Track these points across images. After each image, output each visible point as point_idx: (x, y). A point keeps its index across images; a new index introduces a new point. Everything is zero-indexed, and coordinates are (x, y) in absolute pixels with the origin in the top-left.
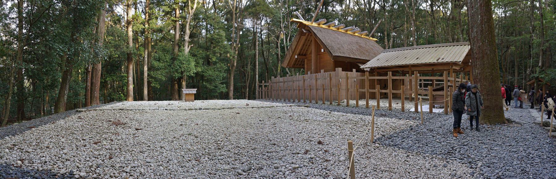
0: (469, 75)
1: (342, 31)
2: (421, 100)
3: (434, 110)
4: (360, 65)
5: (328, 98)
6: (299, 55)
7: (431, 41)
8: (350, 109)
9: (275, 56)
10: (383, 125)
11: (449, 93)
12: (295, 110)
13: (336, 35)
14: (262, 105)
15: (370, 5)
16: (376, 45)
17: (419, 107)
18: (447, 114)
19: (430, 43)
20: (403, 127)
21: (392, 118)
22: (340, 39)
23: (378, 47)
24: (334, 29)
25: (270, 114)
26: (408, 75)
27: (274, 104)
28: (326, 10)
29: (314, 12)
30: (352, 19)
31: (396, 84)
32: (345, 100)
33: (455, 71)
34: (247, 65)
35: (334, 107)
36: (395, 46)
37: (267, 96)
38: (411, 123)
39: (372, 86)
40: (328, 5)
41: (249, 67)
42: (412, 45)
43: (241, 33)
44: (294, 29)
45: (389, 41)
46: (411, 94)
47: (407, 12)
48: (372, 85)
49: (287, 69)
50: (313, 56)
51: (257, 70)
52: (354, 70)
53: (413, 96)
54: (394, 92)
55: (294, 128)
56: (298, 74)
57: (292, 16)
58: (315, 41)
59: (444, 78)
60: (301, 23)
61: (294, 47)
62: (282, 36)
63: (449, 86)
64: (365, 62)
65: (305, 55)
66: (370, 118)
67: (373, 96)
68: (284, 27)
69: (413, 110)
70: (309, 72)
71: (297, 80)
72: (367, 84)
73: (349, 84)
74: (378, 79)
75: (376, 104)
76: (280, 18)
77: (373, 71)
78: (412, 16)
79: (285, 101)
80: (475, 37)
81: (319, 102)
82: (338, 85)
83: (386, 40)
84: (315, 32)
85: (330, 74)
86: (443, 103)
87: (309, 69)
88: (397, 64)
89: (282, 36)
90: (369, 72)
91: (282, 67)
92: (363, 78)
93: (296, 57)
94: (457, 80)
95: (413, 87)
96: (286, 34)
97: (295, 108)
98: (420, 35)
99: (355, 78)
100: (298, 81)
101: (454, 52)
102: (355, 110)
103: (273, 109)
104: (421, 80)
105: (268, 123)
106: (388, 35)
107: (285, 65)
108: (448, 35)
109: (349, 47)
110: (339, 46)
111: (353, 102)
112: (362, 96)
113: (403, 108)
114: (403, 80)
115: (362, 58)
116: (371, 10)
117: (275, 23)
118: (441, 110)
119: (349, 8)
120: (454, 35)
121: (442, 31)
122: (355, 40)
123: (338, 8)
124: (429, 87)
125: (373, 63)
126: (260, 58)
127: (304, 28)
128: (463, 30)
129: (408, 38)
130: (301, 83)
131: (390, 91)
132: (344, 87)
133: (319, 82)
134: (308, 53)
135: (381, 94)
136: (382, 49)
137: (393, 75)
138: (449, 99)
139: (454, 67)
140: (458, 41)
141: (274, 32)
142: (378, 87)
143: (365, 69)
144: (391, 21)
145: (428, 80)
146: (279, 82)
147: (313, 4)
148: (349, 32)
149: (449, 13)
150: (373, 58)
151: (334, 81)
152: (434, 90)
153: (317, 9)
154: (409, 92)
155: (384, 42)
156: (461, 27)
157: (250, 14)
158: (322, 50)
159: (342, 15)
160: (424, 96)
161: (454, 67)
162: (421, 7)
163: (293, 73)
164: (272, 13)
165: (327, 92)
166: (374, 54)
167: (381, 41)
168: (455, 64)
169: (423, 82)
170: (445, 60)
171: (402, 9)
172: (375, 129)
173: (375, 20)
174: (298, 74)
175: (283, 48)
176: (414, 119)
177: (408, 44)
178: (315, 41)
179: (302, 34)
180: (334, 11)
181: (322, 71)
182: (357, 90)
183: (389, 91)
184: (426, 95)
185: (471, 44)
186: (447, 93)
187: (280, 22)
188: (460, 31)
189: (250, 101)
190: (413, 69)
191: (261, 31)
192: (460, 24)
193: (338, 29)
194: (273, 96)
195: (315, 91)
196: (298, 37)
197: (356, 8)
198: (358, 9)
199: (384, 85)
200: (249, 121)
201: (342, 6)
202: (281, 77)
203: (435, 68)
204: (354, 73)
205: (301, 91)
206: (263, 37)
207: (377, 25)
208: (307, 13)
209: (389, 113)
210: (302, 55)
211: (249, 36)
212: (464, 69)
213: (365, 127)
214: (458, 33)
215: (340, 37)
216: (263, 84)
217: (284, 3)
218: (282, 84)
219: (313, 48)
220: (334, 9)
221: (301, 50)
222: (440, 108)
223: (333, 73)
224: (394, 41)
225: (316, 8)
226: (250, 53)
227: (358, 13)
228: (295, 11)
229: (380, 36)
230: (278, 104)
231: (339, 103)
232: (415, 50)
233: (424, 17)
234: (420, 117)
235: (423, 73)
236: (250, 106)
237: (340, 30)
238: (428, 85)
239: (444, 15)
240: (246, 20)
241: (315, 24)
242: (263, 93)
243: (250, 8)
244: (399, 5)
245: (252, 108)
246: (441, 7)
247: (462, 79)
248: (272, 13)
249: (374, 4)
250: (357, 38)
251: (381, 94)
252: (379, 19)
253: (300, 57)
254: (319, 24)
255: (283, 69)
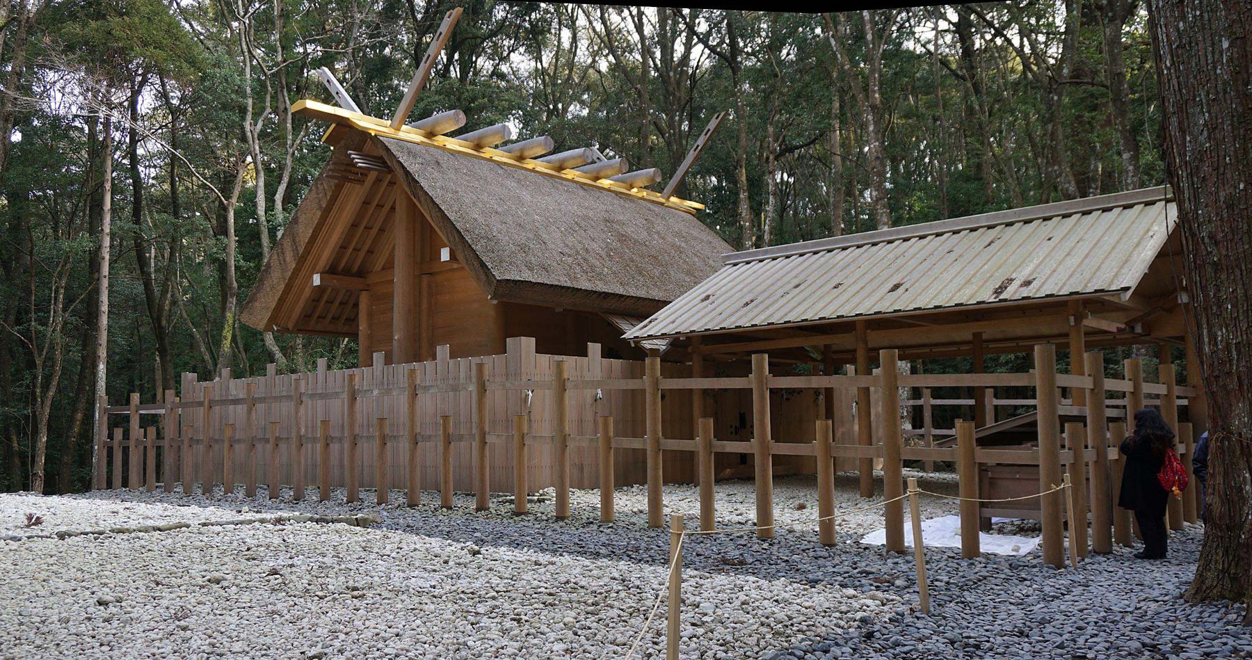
0: (1181, 355)
1: (540, 166)
2: (912, 489)
3: (989, 543)
4: (623, 325)
5: (466, 484)
6: (331, 271)
7: (963, 199)
8: (571, 533)
9: (208, 270)
10: (726, 612)
11: (1066, 456)
12: (303, 539)
13: (512, 184)
14: (118, 521)
15: (667, 51)
16: (700, 232)
17: (908, 526)
18: (1059, 565)
19: (958, 208)
20: (826, 625)
21: (771, 577)
22: (526, 203)
23: (708, 241)
24: (499, 156)
25: (160, 566)
26: (850, 368)
27: (193, 513)
28: (464, 72)
29: (407, 77)
30: (585, 112)
31: (792, 414)
32: (551, 491)
33: (1095, 340)
34: (43, 307)
35: (494, 525)
36: (789, 232)
37: (157, 473)
38: (869, 603)
39: (679, 424)
40: (476, 50)
41: (58, 317)
42: (872, 225)
43: (17, 137)
44: (312, 149)
45: (757, 209)
46: (870, 463)
47: (843, 75)
48: (679, 414)
49: (269, 339)
50: (400, 280)
51: (103, 338)
52: (595, 348)
53: (879, 469)
54: (785, 449)
55: (289, 631)
56: (322, 363)
57: (301, 90)
58: (412, 208)
59: (1035, 378)
60: (343, 123)
61: (304, 233)
62: (251, 178)
63: (1064, 419)
64: (644, 309)
65: (361, 273)
66: (666, 573)
67: (681, 472)
68: (263, 135)
69: (877, 537)
70: (378, 357)
71: (319, 393)
72: (653, 414)
73: (571, 414)
74: (706, 392)
75: (696, 509)
76: (240, 91)
77: (686, 351)
78: (866, 89)
79: (250, 494)
80: (1201, 155)
81: (424, 499)
82: (519, 417)
83: (744, 208)
84: (413, 167)
85: (480, 367)
86: (1035, 505)
87: (380, 340)
88: (795, 316)
89: (251, 178)
90: (666, 357)
91: (244, 327)
92: (632, 384)
93: (317, 280)
94: (1110, 384)
95: (880, 431)
96: (268, 170)
97: (303, 533)
98: (909, 173)
99: (595, 384)
100: (323, 396)
101: (1084, 248)
102: (594, 537)
103: (182, 537)
104: (916, 393)
105: (144, 613)
106: (756, 185)
107: (259, 316)
108: (1054, 160)
109: (570, 240)
110: (521, 238)
111: (585, 500)
112: (630, 473)
113: (827, 527)
114: (829, 392)
115: (632, 292)
116: (674, 71)
117: (208, 114)
118: (1028, 545)
119: (571, 65)
120: (1085, 159)
121: (1020, 146)
122: (597, 207)
123: (521, 62)
124: (958, 423)
125: (683, 315)
126: (125, 278)
127: (359, 149)
128: (1135, 131)
129: (849, 193)
130: (338, 407)
131: (764, 446)
132: (544, 426)
133: (426, 403)
134: (377, 270)
135: (722, 460)
136: (725, 249)
137: (776, 370)
138: (1067, 484)
139: (1091, 322)
140: (1110, 184)
141: (204, 154)
142: (705, 425)
143: (647, 345)
144: (765, 120)
145: (955, 392)
146: (223, 402)
147: (405, 38)
148: (570, 174)
149: (1055, 51)
150: (683, 289)
151: (496, 396)
152: (984, 442)
153: (423, 66)
154: (861, 451)
155: (735, 215)
156: (1122, 114)
157: (70, 48)
158: (445, 255)
159: (536, 96)
160: (938, 467)
161: (1091, 322)
162: (909, 45)
163: (300, 359)
164: (193, 63)
165: (466, 450)
166: (689, 273)
167: (720, 214)
168: (1097, 302)
169: (928, 401)
170: (1039, 290)
171: (820, 63)
172: (690, 630)
173: (692, 117)
174: (322, 363)
175: (249, 237)
176: (884, 583)
177: (849, 223)
178: (412, 208)
179: (346, 173)
180: (502, 76)
181: (443, 351)
182: (608, 441)
183: (760, 443)
184: (949, 466)
185: (1178, 199)
186: (1052, 456)
187: (243, 110)
188: (1116, 136)
189: (54, 500)
190: (875, 338)
191: (134, 142)
192: (1117, 99)
193: (521, 158)
194: (187, 471)
195: (404, 445)
196: (328, 186)
197: (603, 66)
198: (613, 69)
199: (734, 417)
200: (36, 608)
201: (538, 58)
202: (237, 374)
203: (990, 330)
204: (592, 367)
205: (335, 447)
206: (147, 173)
207: (701, 141)
208: (373, 82)
209: (759, 552)
210: (347, 272)
211: (62, 160)
212: (1148, 329)
213: (637, 621)
214: (1107, 145)
215: (526, 196)
216: (135, 406)
217: (263, 22)
218: (241, 409)
219: (399, 242)
220: (504, 68)
221: (343, 247)
222: (1022, 530)
223: (491, 362)
224: (782, 210)
225: (417, 61)
226: (65, 245)
227: (611, 86)
228: (317, 63)
229: (718, 189)
230: (212, 512)
231: (519, 502)
232: (883, 249)
233: (928, 87)
234: (913, 575)
235: (925, 359)
236: (48, 527)
237: (530, 164)
238: (956, 412)
239: (1026, 66)
240: (51, 76)
241: (410, 133)
242: (135, 458)
243: (73, 17)
244: (802, 45)
245: (62, 536)
246: (1013, 34)
247: (1144, 385)
248: (193, 63)
249: (688, 47)
250: (610, 198)
251: (722, 460)
252: (713, 110)
253: (335, 282)
254: (431, 135)
255: (249, 338)
